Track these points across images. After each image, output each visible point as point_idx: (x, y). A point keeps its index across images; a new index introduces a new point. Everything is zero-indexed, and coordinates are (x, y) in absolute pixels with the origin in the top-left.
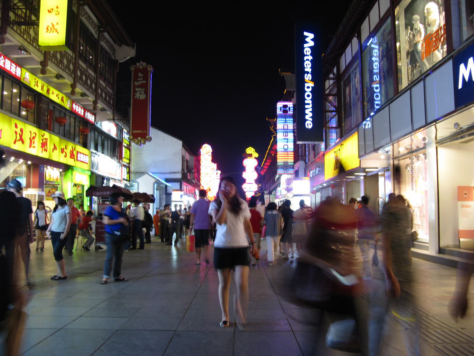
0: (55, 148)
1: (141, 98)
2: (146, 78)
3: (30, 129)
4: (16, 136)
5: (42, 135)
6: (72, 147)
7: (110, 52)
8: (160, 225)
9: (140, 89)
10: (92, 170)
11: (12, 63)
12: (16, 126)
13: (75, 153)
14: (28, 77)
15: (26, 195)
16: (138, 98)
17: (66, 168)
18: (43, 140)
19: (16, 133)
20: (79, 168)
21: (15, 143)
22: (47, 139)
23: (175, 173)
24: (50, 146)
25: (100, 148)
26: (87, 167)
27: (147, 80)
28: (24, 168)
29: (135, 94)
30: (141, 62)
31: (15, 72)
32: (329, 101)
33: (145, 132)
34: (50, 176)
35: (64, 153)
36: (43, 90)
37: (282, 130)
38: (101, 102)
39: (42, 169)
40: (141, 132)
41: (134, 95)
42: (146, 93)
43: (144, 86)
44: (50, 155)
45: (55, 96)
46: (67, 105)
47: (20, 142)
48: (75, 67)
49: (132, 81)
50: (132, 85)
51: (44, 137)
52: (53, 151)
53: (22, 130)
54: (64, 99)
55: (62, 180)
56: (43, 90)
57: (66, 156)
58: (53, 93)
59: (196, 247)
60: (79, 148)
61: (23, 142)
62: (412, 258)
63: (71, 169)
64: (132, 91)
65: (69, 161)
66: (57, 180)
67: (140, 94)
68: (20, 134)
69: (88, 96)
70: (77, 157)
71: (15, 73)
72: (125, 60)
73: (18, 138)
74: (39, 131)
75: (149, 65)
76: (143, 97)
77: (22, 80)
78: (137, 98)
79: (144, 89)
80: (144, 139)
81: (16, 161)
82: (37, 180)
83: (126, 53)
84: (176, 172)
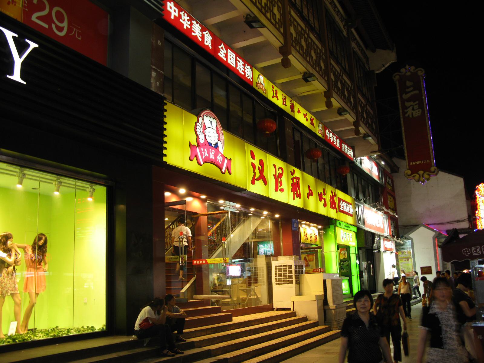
0: (310, 193)
1: (415, 116)
2: (417, 87)
3: (273, 164)
4: (254, 171)
5: (291, 172)
6: (332, 192)
7: (364, 60)
9: (412, 103)
10: (358, 224)
11: (238, 58)
12: (253, 157)
13: (336, 200)
14: (262, 82)
15: (276, 266)
16: (411, 116)
17: (326, 223)
18: (293, 179)
19: (253, 166)
20: (343, 223)
21: (253, 183)
22: (298, 178)
23: (459, 221)
24: (303, 190)
25: (361, 197)
26: (350, 220)
27: (420, 89)
28: (269, 224)
29: (406, 111)
30: (407, 67)
31: (242, 71)
33: (428, 161)
34: (306, 236)
35: (323, 201)
36: (286, 105)
38: (363, 124)
39: (295, 225)
40: (422, 162)
41: (404, 113)
42: (421, 106)
43: (417, 98)
44: (305, 203)
45: (302, 116)
46: (318, 130)
47: (261, 181)
48: (326, 66)
49: (398, 94)
50: (399, 99)
51: (295, 176)
52: (308, 198)
53: (261, 162)
54: (314, 121)
55: (321, 241)
56: (286, 105)
57: (325, 205)
58: (299, 112)
60: (340, 194)
61: (265, 183)
63: (332, 224)
64: (400, 108)
65: (333, 214)
66: (316, 240)
67: (413, 109)
68: (259, 168)
70: (339, 206)
71: (243, 73)
72: (384, 68)
73: (258, 175)
74: (287, 166)
75: (419, 69)
76: (417, 113)
77: (254, 86)
78: (409, 115)
79: (417, 102)
80: (428, 173)
81: (257, 215)
82: (290, 242)
83: (382, 60)
84: (460, 220)
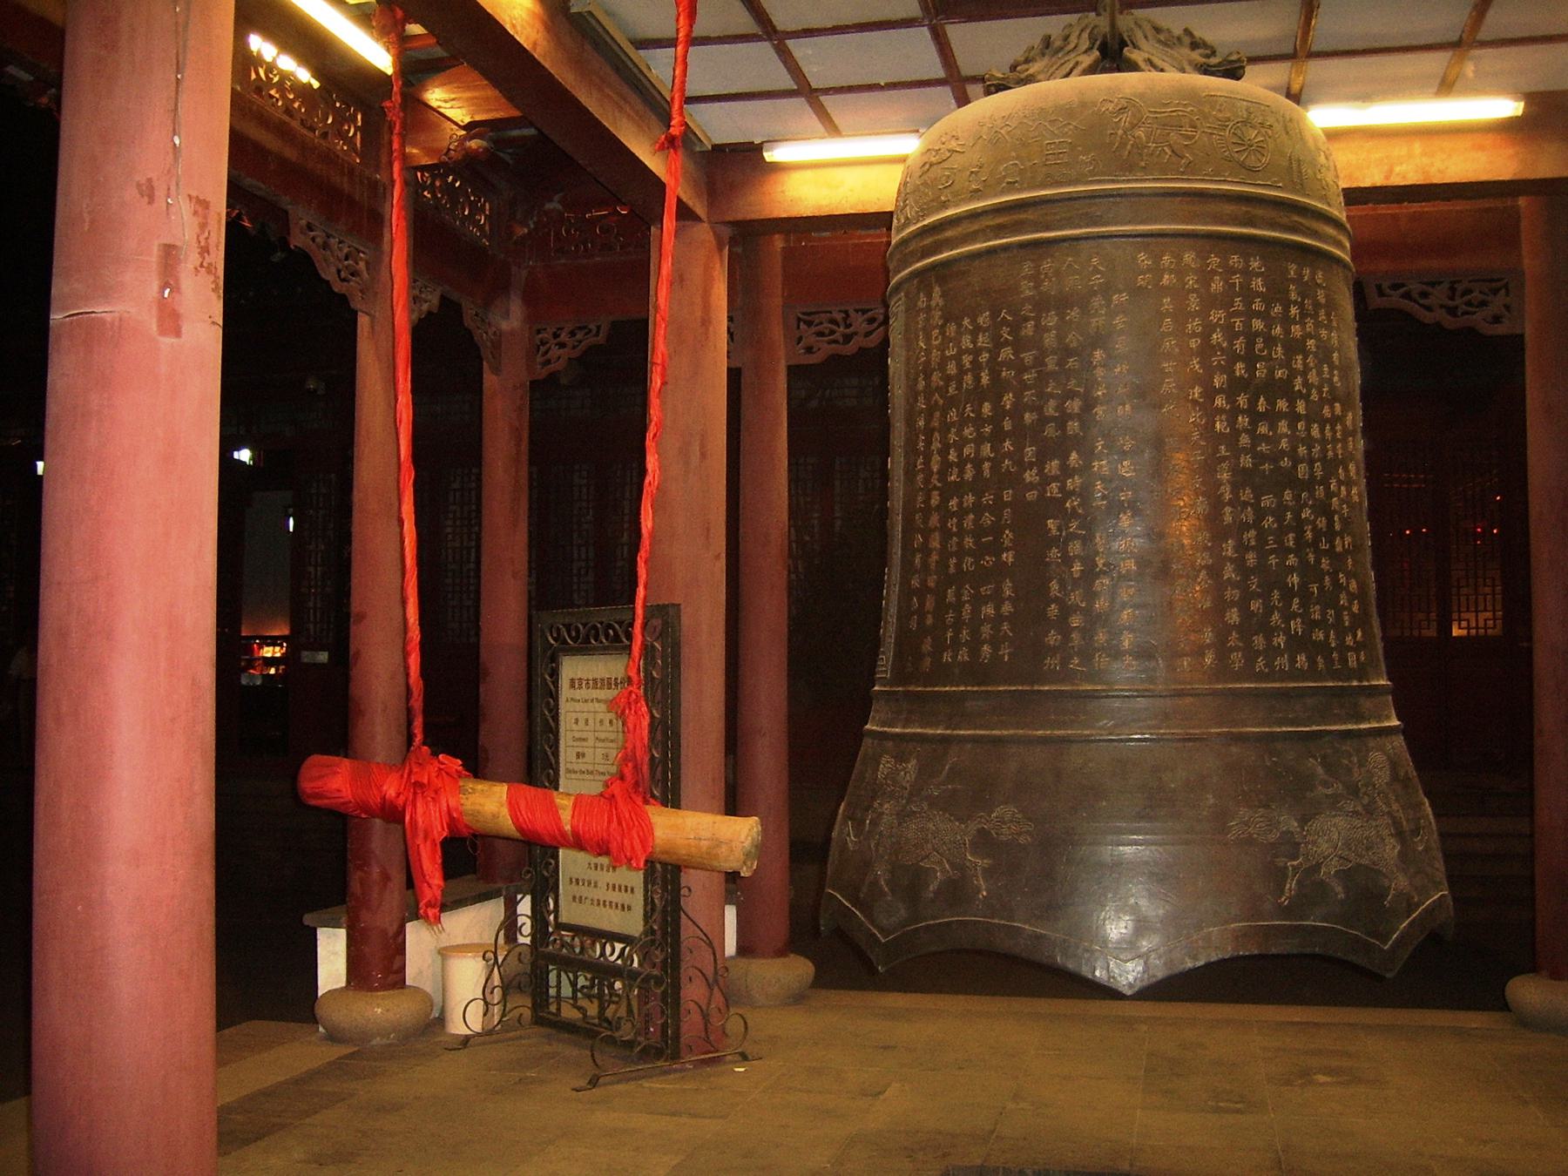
8: (1109, 910)
32: (949, 234)
37: (682, 90)
59: (1522, 336)
62: (390, 71)
69: (679, 200)
